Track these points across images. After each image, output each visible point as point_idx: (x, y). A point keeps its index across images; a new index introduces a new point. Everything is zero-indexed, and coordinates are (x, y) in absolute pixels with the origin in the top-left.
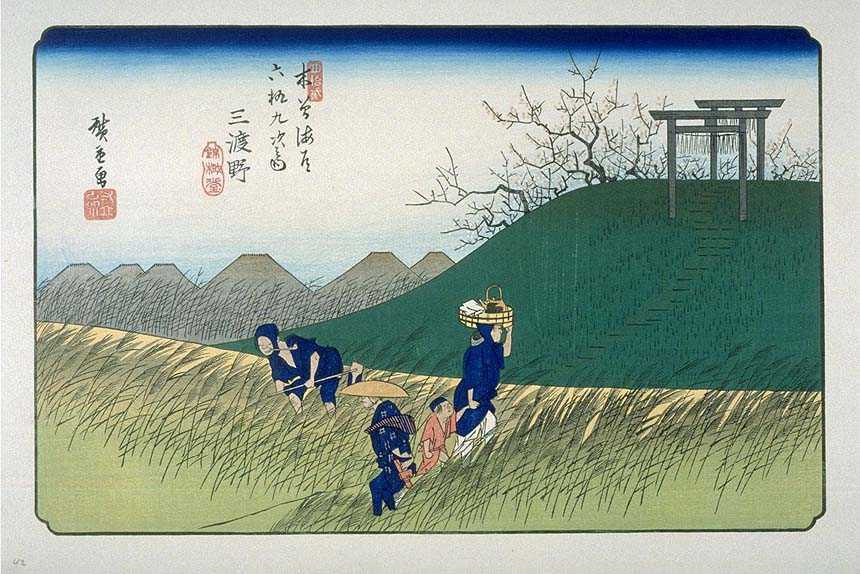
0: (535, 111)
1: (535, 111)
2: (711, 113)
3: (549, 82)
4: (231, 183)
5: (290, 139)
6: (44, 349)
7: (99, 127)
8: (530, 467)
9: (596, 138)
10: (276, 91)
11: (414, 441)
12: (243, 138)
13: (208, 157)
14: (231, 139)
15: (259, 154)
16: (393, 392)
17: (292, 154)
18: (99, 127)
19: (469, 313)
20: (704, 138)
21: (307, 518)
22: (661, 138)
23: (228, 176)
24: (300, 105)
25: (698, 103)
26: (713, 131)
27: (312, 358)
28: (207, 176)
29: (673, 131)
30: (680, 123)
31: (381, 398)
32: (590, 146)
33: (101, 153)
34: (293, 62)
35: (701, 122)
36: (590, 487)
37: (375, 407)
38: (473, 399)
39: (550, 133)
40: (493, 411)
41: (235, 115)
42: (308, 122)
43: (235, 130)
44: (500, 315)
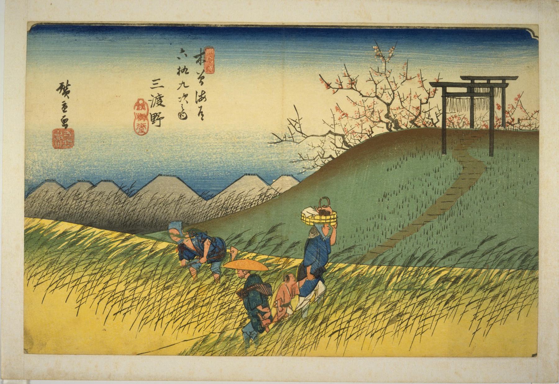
0: (353, 82)
1: (353, 82)
2: (472, 87)
3: (361, 66)
4: (153, 128)
5: (192, 98)
6: (33, 240)
7: (64, 89)
8: (347, 318)
9: (393, 99)
10: (182, 67)
11: (271, 301)
12: (160, 98)
13: (138, 109)
14: (152, 98)
15: (169, 112)
16: (256, 267)
17: (192, 108)
18: (64, 89)
19: (307, 215)
20: (466, 101)
21: (203, 348)
22: (437, 100)
23: (151, 123)
24: (199, 76)
25: (463, 78)
26: (471, 93)
27: (205, 243)
28: (137, 122)
29: (445, 95)
30: (450, 90)
31: (249, 271)
32: (388, 105)
33: (65, 106)
34: (195, 46)
35: (464, 90)
36: (386, 332)
37: (247, 276)
38: (311, 273)
39: (363, 96)
40: (323, 282)
41: (155, 82)
42: (203, 88)
43: (155, 93)
44: (328, 217)
